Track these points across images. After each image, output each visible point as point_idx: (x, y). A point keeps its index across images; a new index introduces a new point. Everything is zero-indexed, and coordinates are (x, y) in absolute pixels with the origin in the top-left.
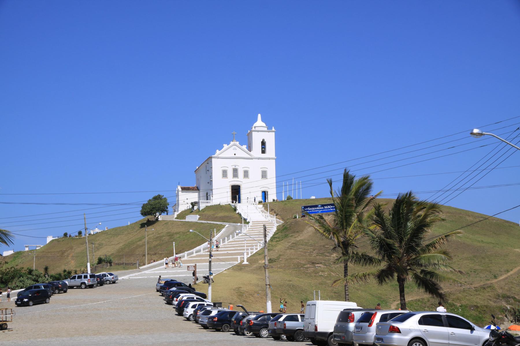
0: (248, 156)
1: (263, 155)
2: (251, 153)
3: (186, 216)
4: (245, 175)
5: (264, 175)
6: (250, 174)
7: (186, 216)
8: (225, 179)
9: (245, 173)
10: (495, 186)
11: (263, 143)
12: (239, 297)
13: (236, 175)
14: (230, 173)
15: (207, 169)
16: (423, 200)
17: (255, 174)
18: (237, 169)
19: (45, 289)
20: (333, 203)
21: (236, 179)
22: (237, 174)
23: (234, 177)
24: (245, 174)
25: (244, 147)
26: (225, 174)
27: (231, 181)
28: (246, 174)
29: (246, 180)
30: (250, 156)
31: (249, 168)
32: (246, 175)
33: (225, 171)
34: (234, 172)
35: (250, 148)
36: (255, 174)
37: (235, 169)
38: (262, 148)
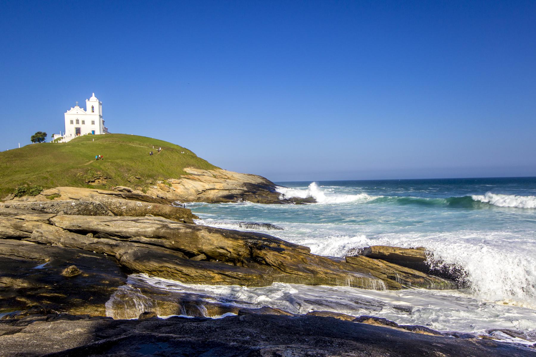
0: (85, 114)
3: (65, 113)
5: (93, 123)
6: (85, 122)
7: (65, 113)
8: (72, 125)
11: (93, 107)
12: (154, 315)
14: (75, 122)
15: (76, 113)
17: (88, 122)
21: (78, 125)
25: (82, 109)
26: (72, 122)
27: (75, 125)
28: (83, 122)
29: (83, 125)
33: (431, 253)
35: (85, 110)
36: (88, 122)
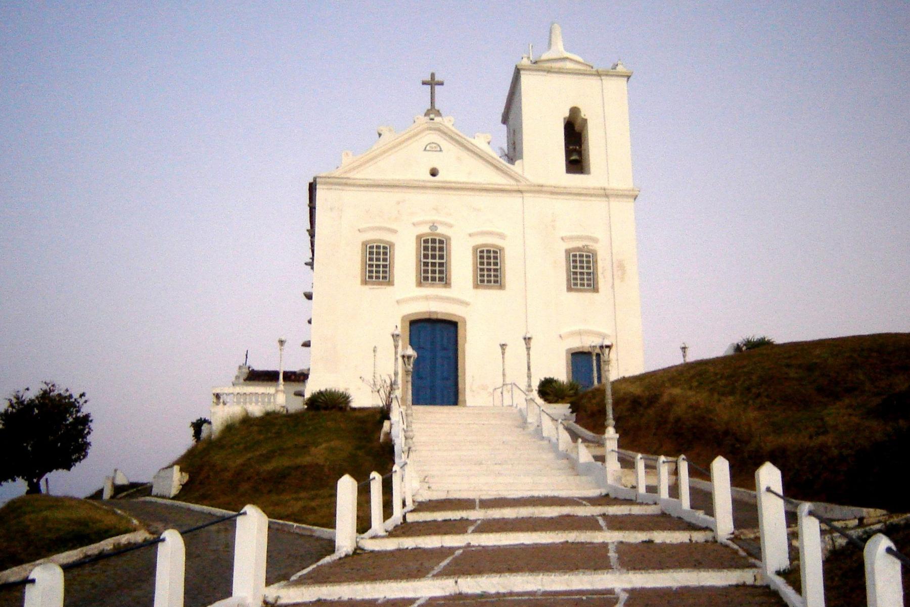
1: (576, 180)
2: (517, 167)
4: (482, 270)
9: (441, 265)
10: (529, 369)
13: (492, 273)
16: (418, 595)
18: (441, 242)
19: (630, 453)
20: (152, 494)
21: (438, 291)
22: (496, 270)
23: (426, 279)
24: (579, 270)
30: (513, 182)
31: (394, 232)
32: (582, 273)
34: (426, 256)
37: (434, 241)
38: (568, 153)
